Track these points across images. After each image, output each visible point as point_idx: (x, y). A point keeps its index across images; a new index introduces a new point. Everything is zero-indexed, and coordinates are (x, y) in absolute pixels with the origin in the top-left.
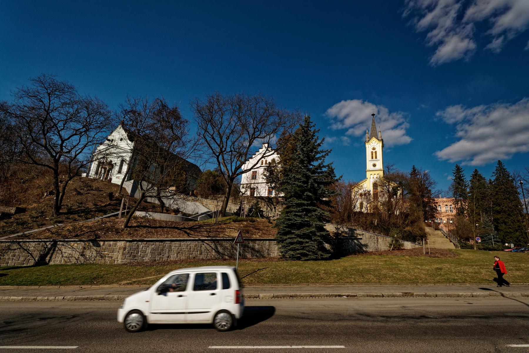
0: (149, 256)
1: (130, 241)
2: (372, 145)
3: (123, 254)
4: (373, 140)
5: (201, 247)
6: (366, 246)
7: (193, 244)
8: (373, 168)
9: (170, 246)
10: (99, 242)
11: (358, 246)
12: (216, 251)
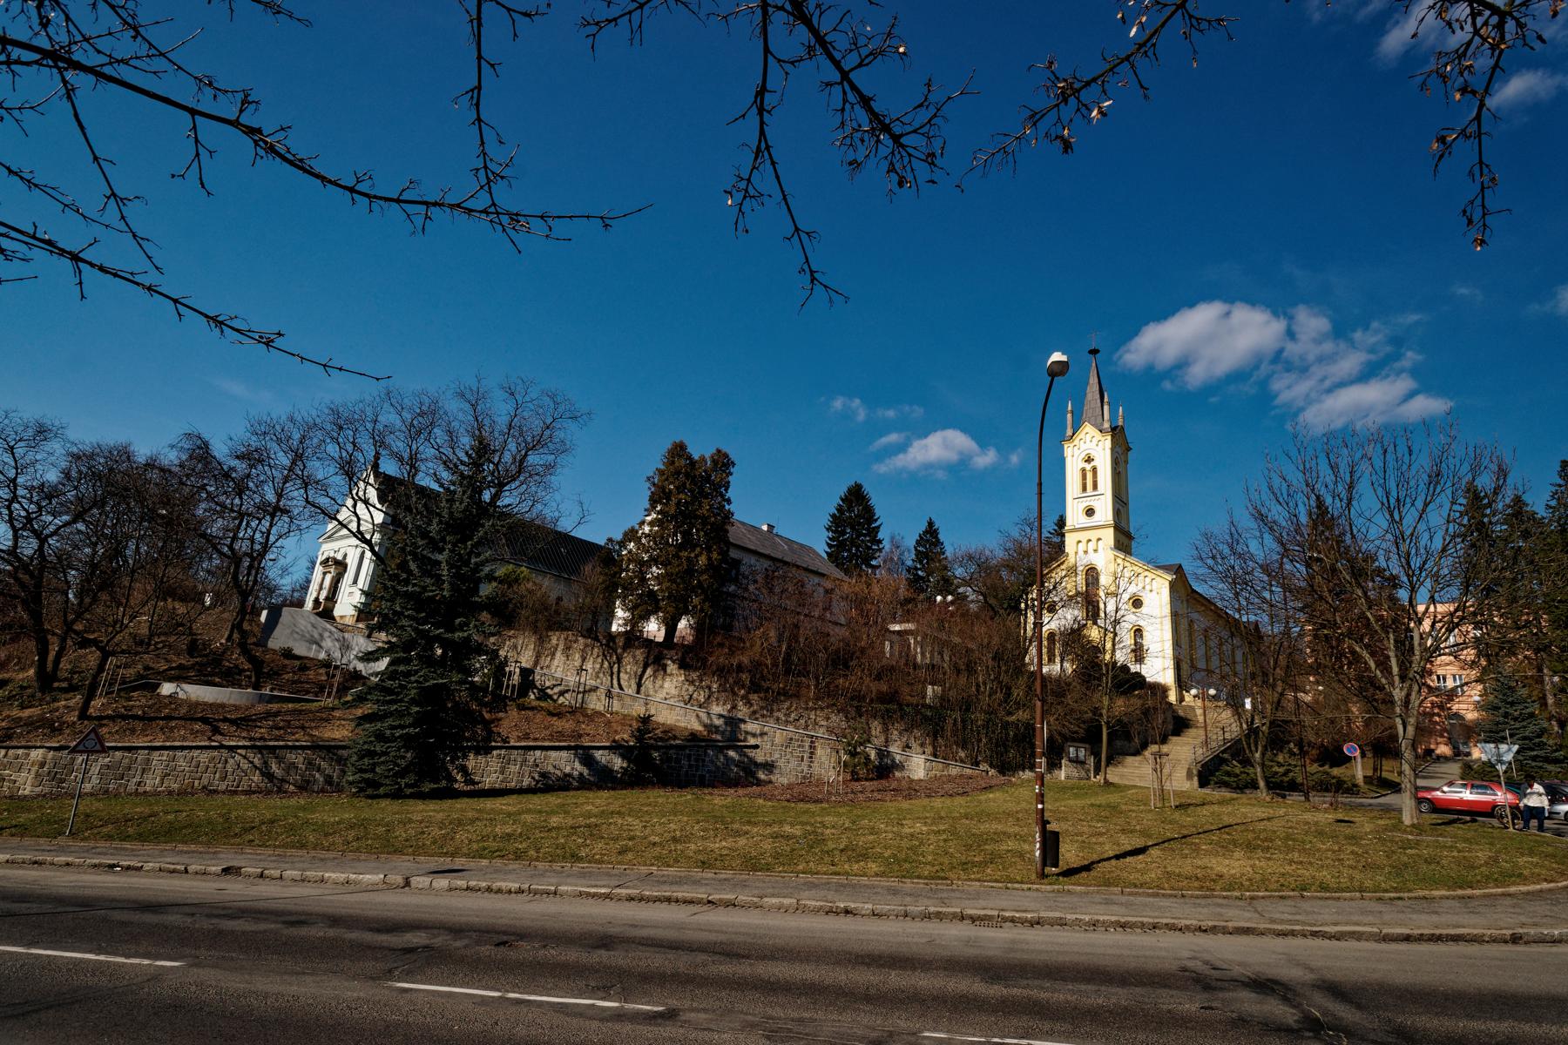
0: (95, 781)
1: (55, 749)
3: (37, 775)
4: (1085, 431)
5: (226, 762)
6: (769, 767)
7: (204, 757)
8: (1084, 521)
9: (148, 759)
11: (736, 766)
12: (263, 774)
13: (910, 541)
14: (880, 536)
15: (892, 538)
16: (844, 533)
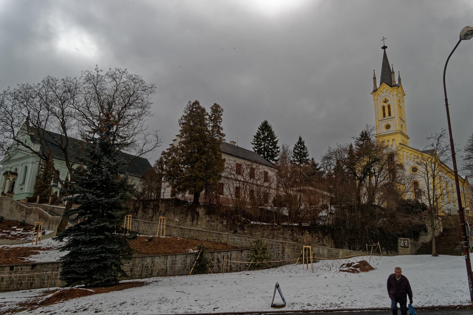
2: (382, 95)
4: (383, 87)
10: (64, 183)
13: (291, 148)
14: (278, 145)
15: (283, 147)
16: (261, 145)
